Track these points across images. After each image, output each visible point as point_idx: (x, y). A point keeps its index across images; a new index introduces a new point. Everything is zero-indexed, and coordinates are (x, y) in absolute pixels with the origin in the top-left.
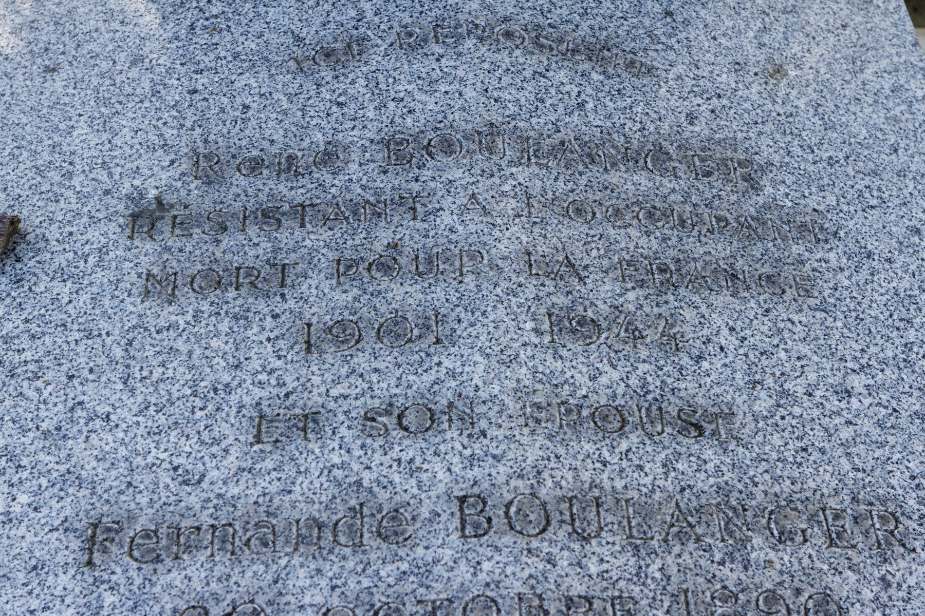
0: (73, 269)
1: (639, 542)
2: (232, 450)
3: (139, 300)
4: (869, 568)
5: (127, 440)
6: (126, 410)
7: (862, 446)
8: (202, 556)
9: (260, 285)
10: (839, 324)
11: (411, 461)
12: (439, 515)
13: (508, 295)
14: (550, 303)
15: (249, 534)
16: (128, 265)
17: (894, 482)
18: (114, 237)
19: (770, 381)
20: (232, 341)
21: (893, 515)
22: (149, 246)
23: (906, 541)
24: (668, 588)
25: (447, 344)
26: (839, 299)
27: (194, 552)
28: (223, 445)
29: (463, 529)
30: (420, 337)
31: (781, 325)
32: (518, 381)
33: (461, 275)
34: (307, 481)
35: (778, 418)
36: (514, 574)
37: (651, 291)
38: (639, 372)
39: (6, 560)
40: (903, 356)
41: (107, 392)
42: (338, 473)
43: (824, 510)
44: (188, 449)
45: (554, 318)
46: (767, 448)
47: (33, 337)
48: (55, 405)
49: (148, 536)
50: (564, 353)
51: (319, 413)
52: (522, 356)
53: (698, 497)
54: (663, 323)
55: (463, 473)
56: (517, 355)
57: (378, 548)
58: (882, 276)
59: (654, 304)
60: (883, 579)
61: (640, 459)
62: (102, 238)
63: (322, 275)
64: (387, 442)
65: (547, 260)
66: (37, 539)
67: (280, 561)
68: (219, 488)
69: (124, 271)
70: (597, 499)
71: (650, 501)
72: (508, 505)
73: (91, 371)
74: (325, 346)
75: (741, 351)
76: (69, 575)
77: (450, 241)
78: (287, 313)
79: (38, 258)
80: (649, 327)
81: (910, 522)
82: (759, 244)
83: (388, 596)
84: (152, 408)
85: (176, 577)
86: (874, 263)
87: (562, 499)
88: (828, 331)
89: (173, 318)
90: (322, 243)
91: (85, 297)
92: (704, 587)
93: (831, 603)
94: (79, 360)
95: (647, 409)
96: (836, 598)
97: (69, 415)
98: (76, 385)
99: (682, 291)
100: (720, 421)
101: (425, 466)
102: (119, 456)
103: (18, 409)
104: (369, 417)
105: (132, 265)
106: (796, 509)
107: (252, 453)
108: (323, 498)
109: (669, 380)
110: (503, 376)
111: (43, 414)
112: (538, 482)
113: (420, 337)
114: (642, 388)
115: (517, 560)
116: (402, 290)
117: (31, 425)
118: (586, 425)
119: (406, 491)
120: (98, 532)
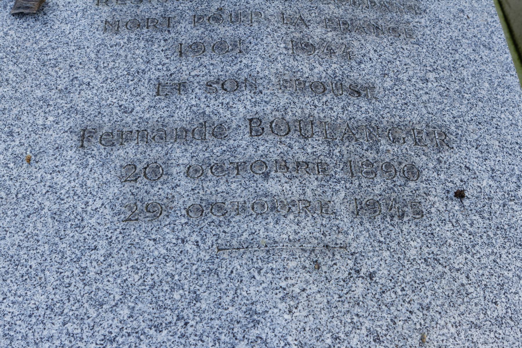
0: (71, 19)
1: (330, 140)
2: (146, 98)
3: (102, 33)
4: (432, 155)
5: (98, 93)
6: (97, 81)
7: (432, 103)
8: (133, 143)
9: (158, 27)
10: (424, 50)
11: (228, 103)
12: (240, 127)
13: (273, 32)
14: (292, 36)
15: (154, 134)
16: (96, 17)
17: (445, 119)
18: (90, 4)
19: (392, 74)
20: (145, 51)
21: (444, 133)
22: (106, 8)
23: (449, 144)
24: (343, 160)
25: (244, 53)
26: (425, 40)
27: (130, 141)
28: (142, 96)
29: (251, 132)
30: (232, 50)
31: (398, 50)
32: (277, 69)
33: (252, 22)
34: (181, 112)
35: (394, 90)
36: (274, 151)
37: (339, 33)
38: (332, 68)
39: (44, 145)
40: (453, 65)
41: (88, 73)
42: (194, 108)
43: (413, 130)
44: (126, 98)
45: (294, 43)
46: (389, 103)
47: (53, 48)
48: (64, 78)
49: (108, 135)
50: (298, 58)
51: (186, 82)
52: (279, 59)
53: (357, 122)
54: (344, 47)
55: (251, 109)
56: (277, 58)
57: (213, 140)
58: (445, 30)
59: (340, 38)
60: (438, 159)
61: (332, 105)
62: (84, 5)
63: (187, 22)
64: (217, 95)
65: (291, 17)
66: (58, 136)
67: (168, 146)
68: (140, 115)
69: (95, 20)
70: (312, 121)
71: (335, 123)
72: (272, 123)
73: (80, 64)
74: (188, 54)
75: (379, 61)
76: (73, 151)
77: (246, 8)
78: (171, 39)
79: (54, 14)
80: (337, 48)
81: (451, 136)
82: (389, 14)
83: (217, 161)
84: (109, 80)
85: (121, 152)
86: (442, 25)
87: (296, 121)
88: (419, 53)
89: (118, 41)
90: (187, 8)
91: (77, 31)
92: (359, 160)
93: (415, 169)
94: (75, 59)
95: (336, 84)
96: (417, 166)
97: (71, 83)
98: (74, 70)
99: (353, 33)
100: (368, 90)
101: (234, 106)
102: (94, 101)
103: (47, 80)
104: (209, 85)
105: (98, 17)
106: (401, 129)
107: (155, 100)
108: (188, 119)
109: (346, 72)
110: (270, 67)
111: (59, 82)
112: (285, 113)
113: (232, 50)
114: (334, 75)
115: (275, 146)
116: (224, 29)
117: (53, 87)
118: (307, 90)
119: (225, 116)
120: (86, 133)
